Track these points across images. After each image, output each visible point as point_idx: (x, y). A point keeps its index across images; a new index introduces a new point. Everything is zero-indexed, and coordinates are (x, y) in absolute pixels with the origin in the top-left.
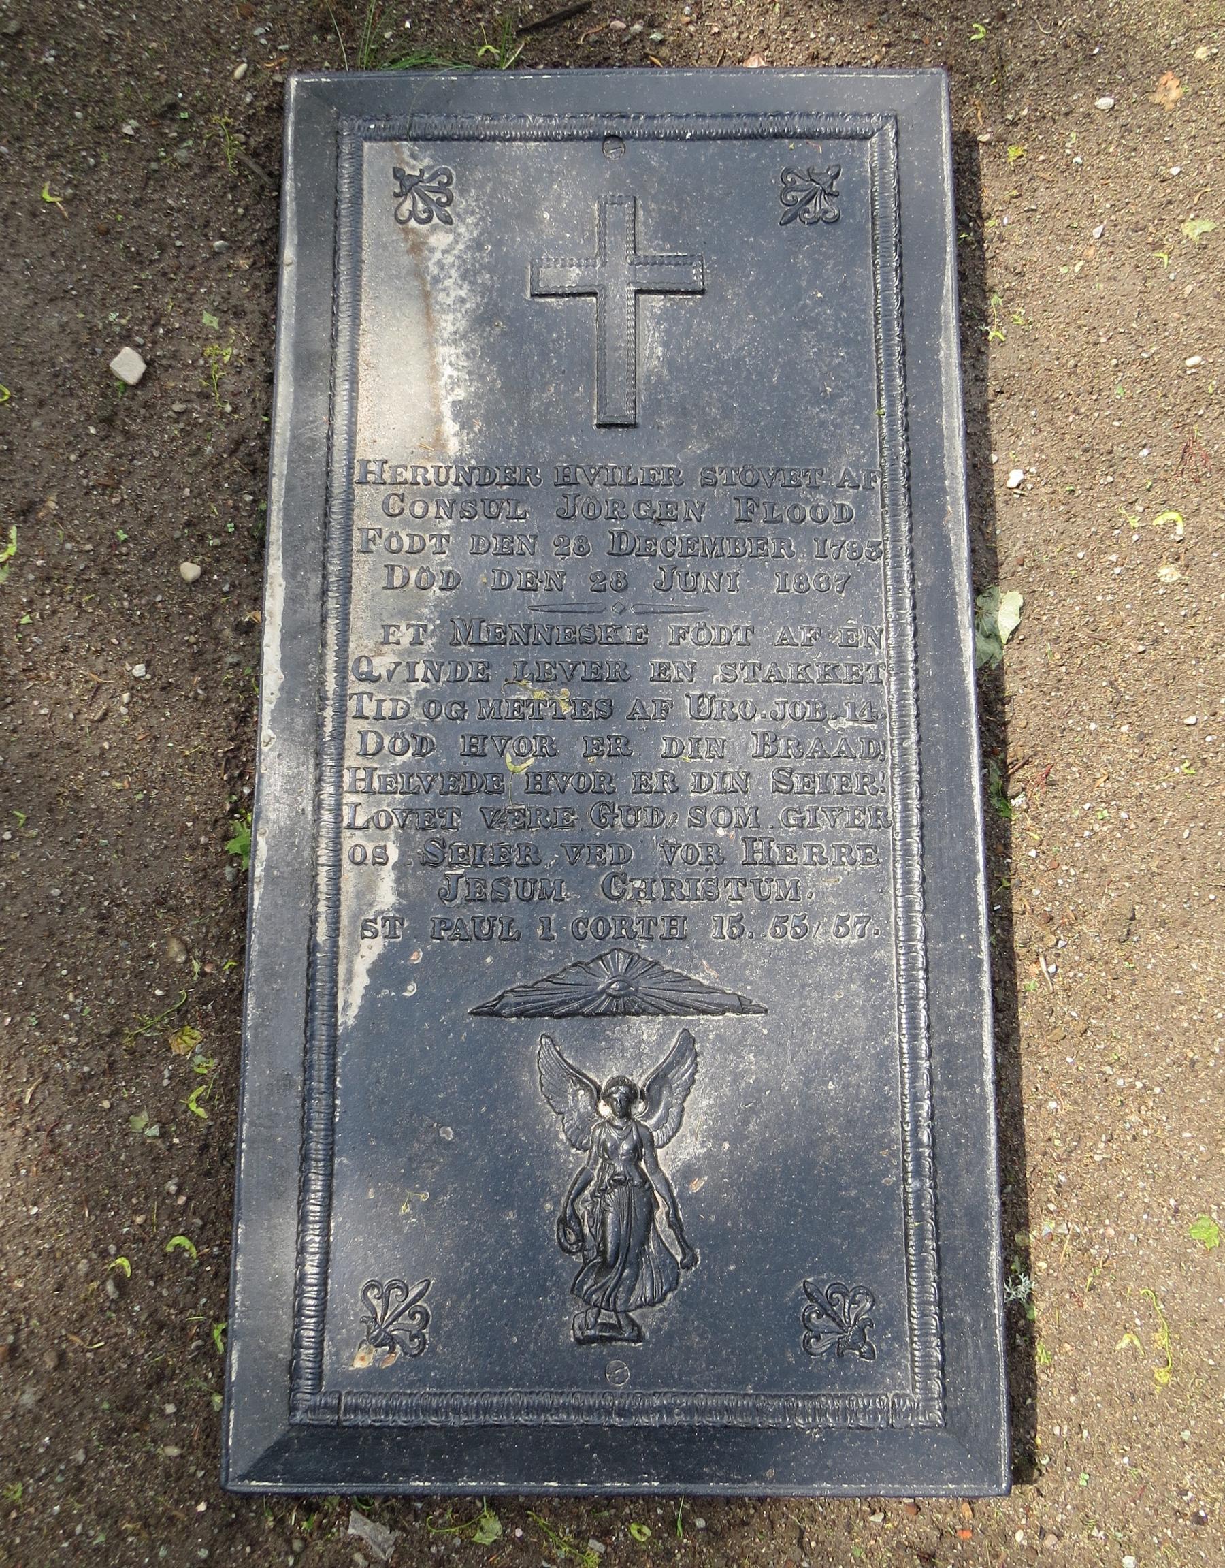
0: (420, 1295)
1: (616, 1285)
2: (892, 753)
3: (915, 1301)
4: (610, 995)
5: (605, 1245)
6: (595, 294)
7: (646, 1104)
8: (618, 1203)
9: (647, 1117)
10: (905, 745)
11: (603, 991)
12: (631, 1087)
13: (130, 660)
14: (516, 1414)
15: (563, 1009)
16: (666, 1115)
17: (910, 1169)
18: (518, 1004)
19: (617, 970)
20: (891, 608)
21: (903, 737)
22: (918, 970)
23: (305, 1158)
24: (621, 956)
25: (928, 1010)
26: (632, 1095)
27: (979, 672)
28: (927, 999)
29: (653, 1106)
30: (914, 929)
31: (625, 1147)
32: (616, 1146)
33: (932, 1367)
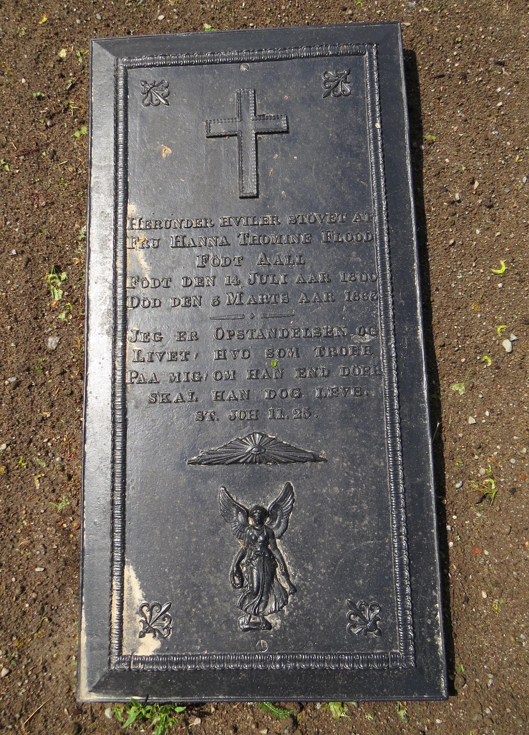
0: (167, 610)
1: (259, 604)
2: (383, 350)
3: (388, 409)
4: (252, 454)
5: (253, 585)
6: (236, 135)
7: (270, 518)
8: (258, 565)
9: (271, 524)
10: (389, 344)
11: (249, 452)
12: (263, 510)
13: (26, 694)
14: (213, 664)
15: (230, 461)
16: (280, 522)
17: (396, 546)
18: (209, 459)
19: (255, 443)
20: (378, 241)
21: (388, 340)
22: (396, 423)
23: (112, 575)
24: (257, 435)
25: (403, 470)
26: (264, 514)
27: (405, 52)
28: (400, 424)
29: (274, 519)
30: (396, 446)
31: (261, 538)
32: (257, 538)
33: (402, 535)
